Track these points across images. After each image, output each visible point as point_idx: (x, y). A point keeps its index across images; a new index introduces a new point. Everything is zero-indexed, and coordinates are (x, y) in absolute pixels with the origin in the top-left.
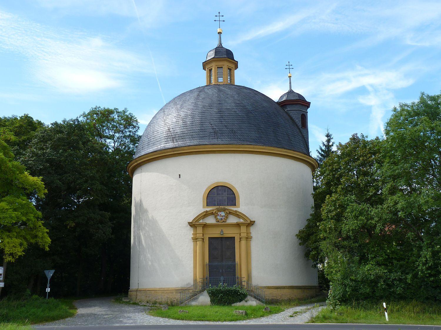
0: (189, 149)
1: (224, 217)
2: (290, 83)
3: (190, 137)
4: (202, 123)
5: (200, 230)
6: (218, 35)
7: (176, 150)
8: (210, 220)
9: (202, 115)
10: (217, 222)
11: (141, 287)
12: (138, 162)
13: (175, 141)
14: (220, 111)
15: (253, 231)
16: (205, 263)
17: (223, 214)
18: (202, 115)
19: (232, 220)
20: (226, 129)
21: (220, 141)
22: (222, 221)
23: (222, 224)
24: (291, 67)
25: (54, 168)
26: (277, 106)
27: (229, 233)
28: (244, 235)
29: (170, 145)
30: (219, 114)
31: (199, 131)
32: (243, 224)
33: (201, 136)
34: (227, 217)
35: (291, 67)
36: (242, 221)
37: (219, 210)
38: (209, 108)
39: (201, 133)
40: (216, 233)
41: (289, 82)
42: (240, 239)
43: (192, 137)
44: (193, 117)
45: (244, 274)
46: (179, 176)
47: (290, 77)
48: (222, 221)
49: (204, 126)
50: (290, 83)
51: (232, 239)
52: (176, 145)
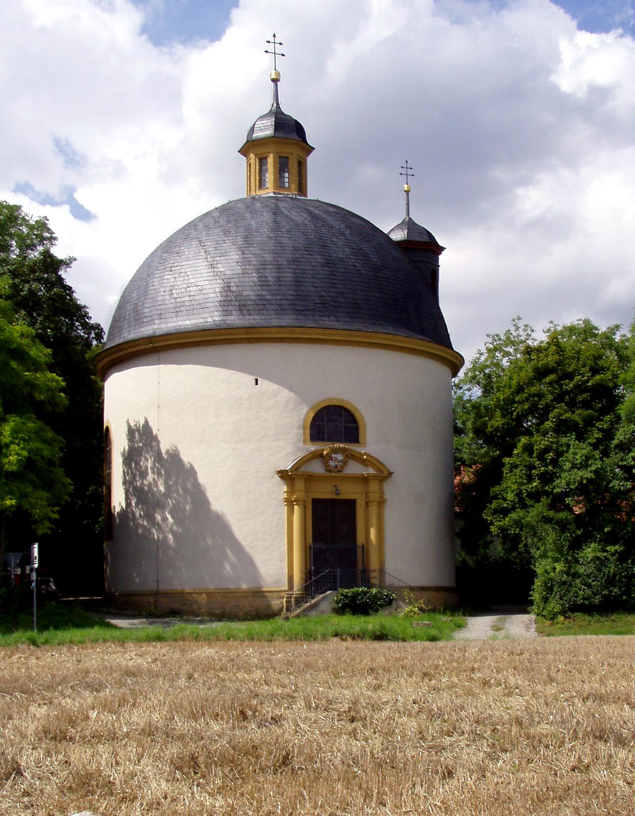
0: (279, 333)
1: (341, 464)
2: (408, 204)
3: (277, 307)
4: (298, 282)
5: (300, 485)
6: (272, 84)
7: (255, 331)
8: (317, 468)
9: (296, 267)
10: (326, 470)
11: (163, 587)
12: (155, 345)
13: (245, 312)
14: (328, 263)
15: (388, 487)
16: (308, 545)
17: (340, 457)
18: (296, 267)
19: (354, 469)
20: (343, 300)
21: (334, 324)
22: (336, 470)
23: (334, 473)
24: (410, 172)
25: (61, 356)
26: (396, 253)
27: (348, 492)
28: (375, 496)
29: (234, 319)
30: (328, 269)
31: (259, 289)
32: (374, 477)
33: (299, 308)
34: (345, 463)
35: (410, 172)
36: (371, 471)
37: (335, 451)
38: (306, 253)
39: (298, 303)
40: (325, 492)
41: (405, 202)
42: (367, 503)
43: (281, 310)
44: (279, 268)
45: (374, 564)
46: (254, 381)
47: (407, 192)
48: (336, 470)
49: (302, 288)
50: (408, 204)
51: (351, 504)
52: (250, 321)
